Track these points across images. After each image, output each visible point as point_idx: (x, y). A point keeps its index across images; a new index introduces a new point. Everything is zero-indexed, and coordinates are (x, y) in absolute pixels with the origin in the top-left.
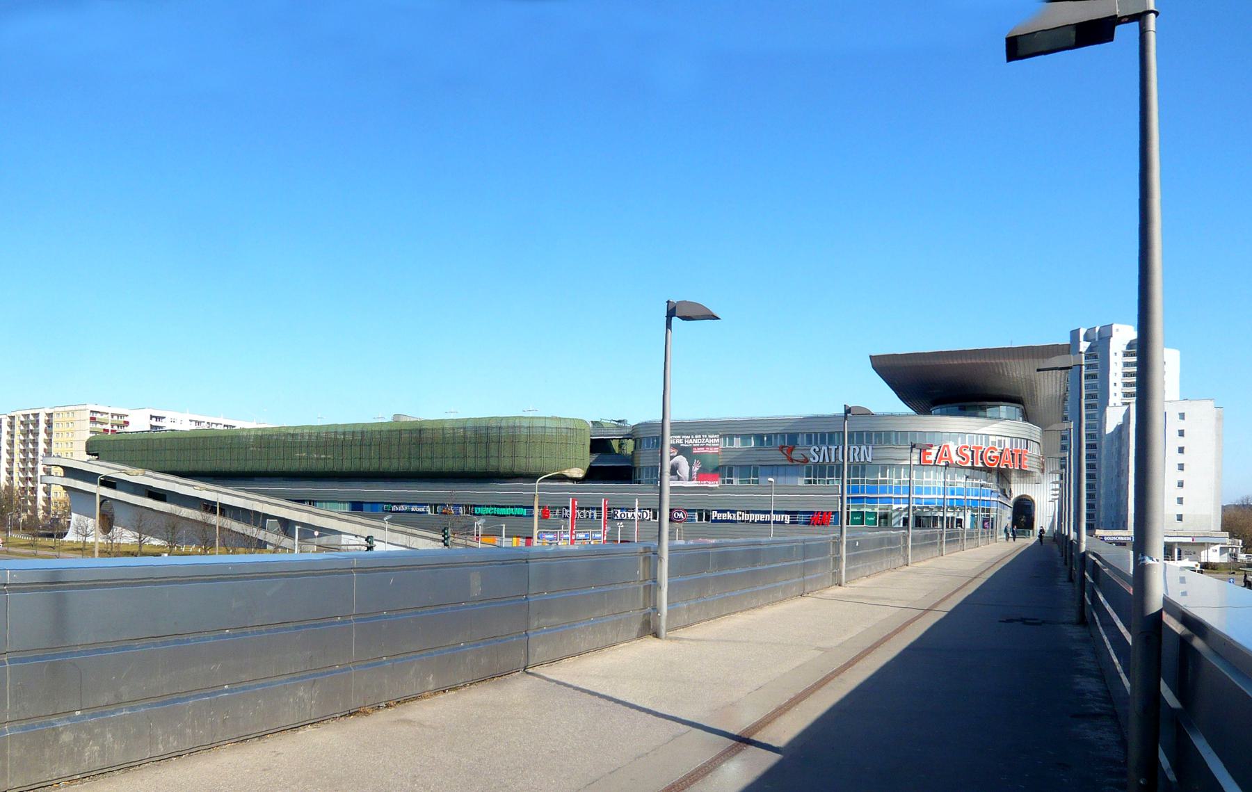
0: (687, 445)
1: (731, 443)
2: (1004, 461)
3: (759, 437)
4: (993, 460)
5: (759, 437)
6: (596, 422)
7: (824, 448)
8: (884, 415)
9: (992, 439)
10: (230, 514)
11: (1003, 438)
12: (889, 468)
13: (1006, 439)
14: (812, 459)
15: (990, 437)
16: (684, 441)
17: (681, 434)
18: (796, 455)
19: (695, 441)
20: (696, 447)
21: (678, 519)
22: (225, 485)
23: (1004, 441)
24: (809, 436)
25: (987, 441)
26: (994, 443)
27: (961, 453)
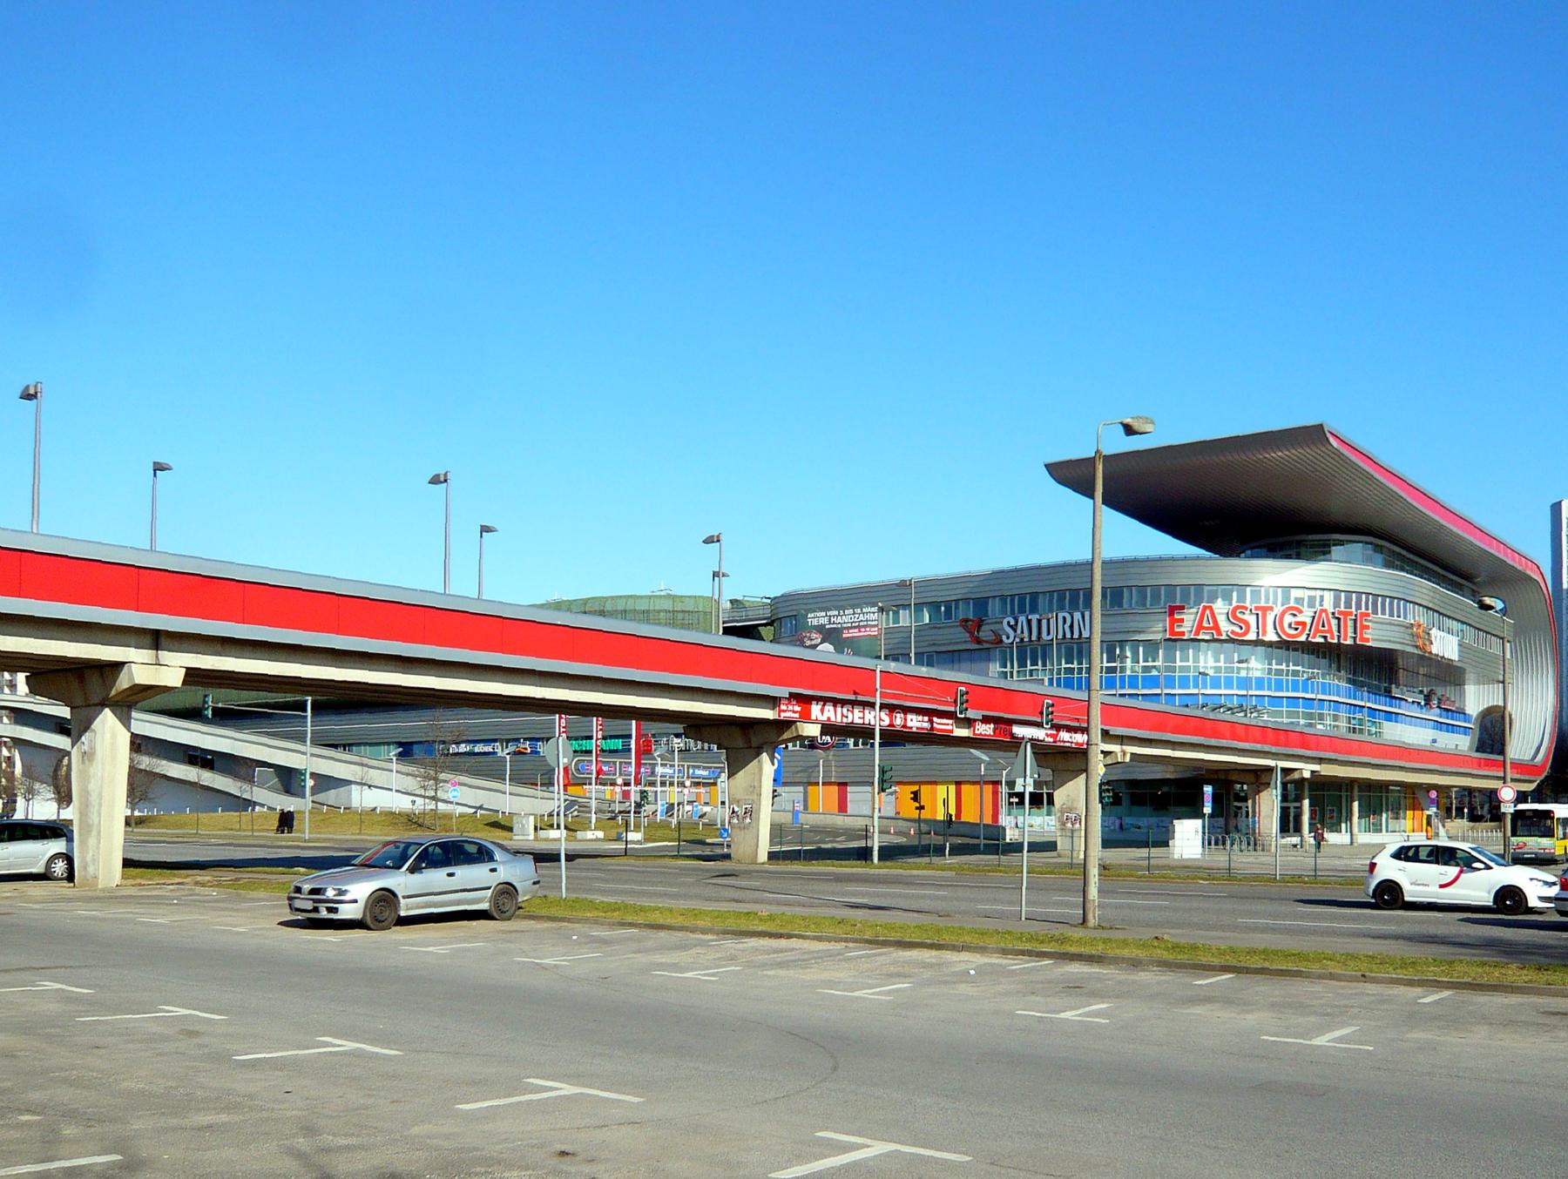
0: (835, 626)
1: (896, 620)
2: (1317, 631)
3: (934, 606)
4: (1297, 629)
5: (934, 606)
6: (736, 601)
7: (1022, 619)
8: (1147, 560)
9: (1295, 593)
10: (147, 749)
11: (1319, 593)
12: (1181, 651)
13: (1326, 594)
14: (1004, 638)
15: (1292, 590)
16: (830, 620)
17: (827, 609)
18: (985, 633)
19: (844, 619)
20: (848, 628)
21: (823, 744)
22: (239, 729)
23: (1322, 597)
24: (1003, 598)
25: (1286, 598)
26: (1299, 600)
27: (1235, 617)
